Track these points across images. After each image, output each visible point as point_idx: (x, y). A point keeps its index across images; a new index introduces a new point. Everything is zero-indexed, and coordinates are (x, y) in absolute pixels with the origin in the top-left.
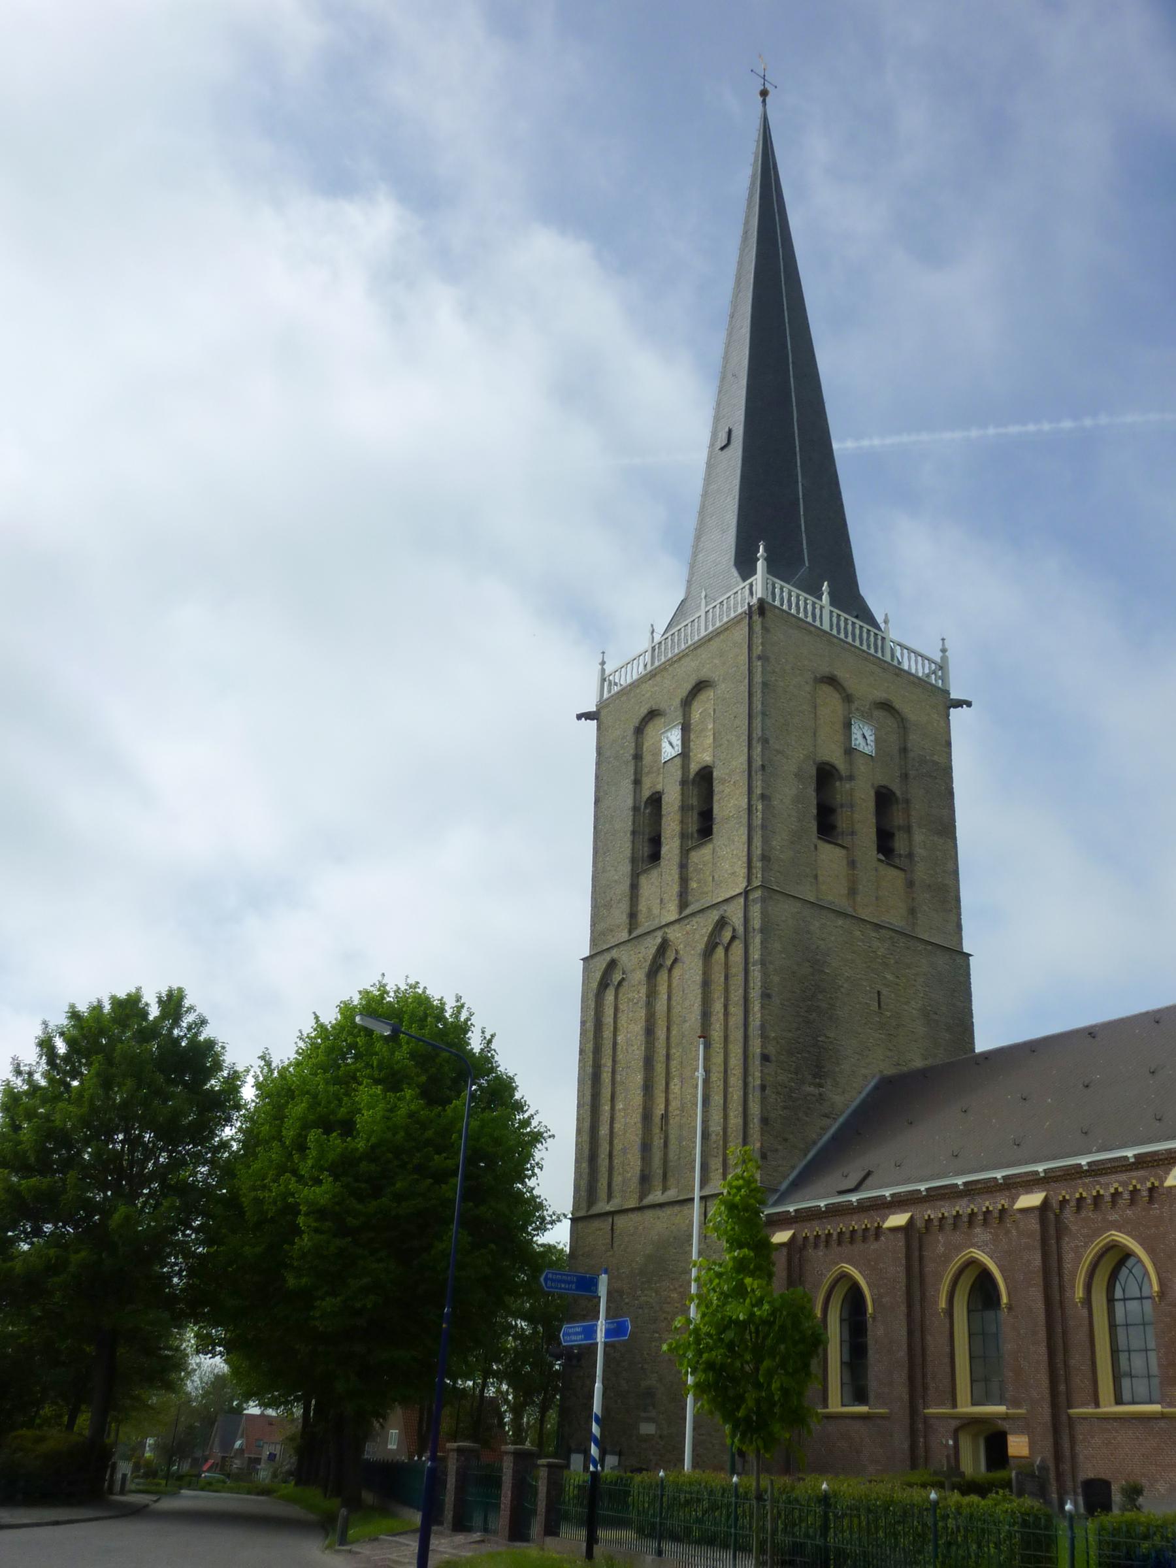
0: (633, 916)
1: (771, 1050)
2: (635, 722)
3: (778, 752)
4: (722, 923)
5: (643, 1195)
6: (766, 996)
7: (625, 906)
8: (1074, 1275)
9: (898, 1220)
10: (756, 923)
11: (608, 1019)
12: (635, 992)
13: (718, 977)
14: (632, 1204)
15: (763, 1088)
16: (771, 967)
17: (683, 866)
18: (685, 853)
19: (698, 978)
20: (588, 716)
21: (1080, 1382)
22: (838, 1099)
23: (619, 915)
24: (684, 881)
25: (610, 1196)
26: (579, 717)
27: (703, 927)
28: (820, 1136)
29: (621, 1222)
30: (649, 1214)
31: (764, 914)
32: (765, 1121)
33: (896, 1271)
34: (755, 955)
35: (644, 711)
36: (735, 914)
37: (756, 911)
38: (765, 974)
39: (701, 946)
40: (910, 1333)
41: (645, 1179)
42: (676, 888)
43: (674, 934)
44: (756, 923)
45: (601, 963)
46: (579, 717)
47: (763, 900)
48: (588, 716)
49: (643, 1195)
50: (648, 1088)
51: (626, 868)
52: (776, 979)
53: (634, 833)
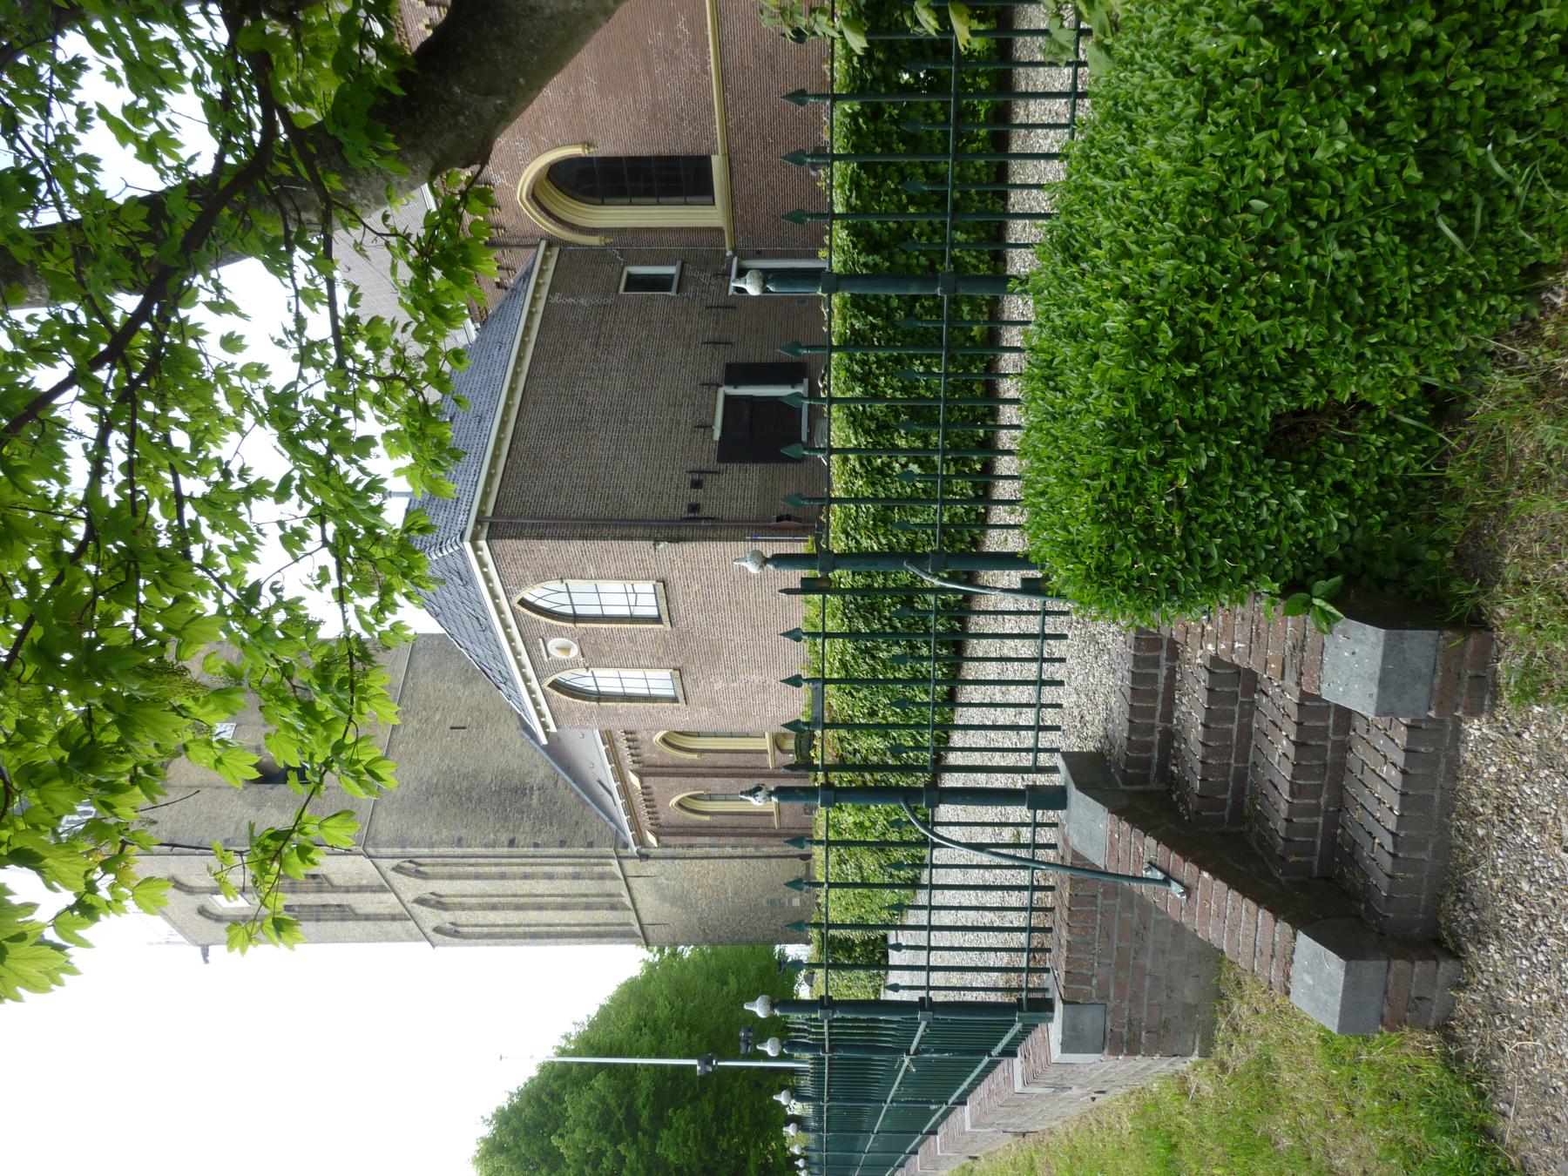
0: (393, 918)
1: (504, 838)
2: (211, 923)
3: (237, 828)
4: (398, 869)
5: (626, 908)
6: (459, 842)
7: (386, 924)
8: (673, 758)
9: (634, 780)
10: (397, 851)
11: (485, 930)
12: (462, 917)
13: (446, 870)
14: (633, 914)
15: (536, 845)
16: (435, 837)
17: (347, 890)
18: (334, 889)
19: (447, 882)
20: (205, 954)
21: (752, 760)
22: (542, 772)
23: (396, 925)
24: (361, 889)
25: (629, 924)
26: (206, 961)
27: (398, 880)
28: (572, 790)
29: (646, 919)
30: (639, 906)
31: (389, 844)
32: (562, 844)
33: (673, 781)
34: (426, 851)
35: (200, 918)
36: (386, 864)
37: (384, 851)
38: (441, 844)
39: (419, 881)
40: (717, 775)
41: (613, 907)
42: (368, 895)
43: (408, 896)
44: (397, 851)
45: (437, 937)
46: (206, 961)
47: (376, 845)
48: (205, 954)
49: (626, 908)
50: (541, 907)
51: (351, 924)
52: (445, 833)
53: (318, 920)
